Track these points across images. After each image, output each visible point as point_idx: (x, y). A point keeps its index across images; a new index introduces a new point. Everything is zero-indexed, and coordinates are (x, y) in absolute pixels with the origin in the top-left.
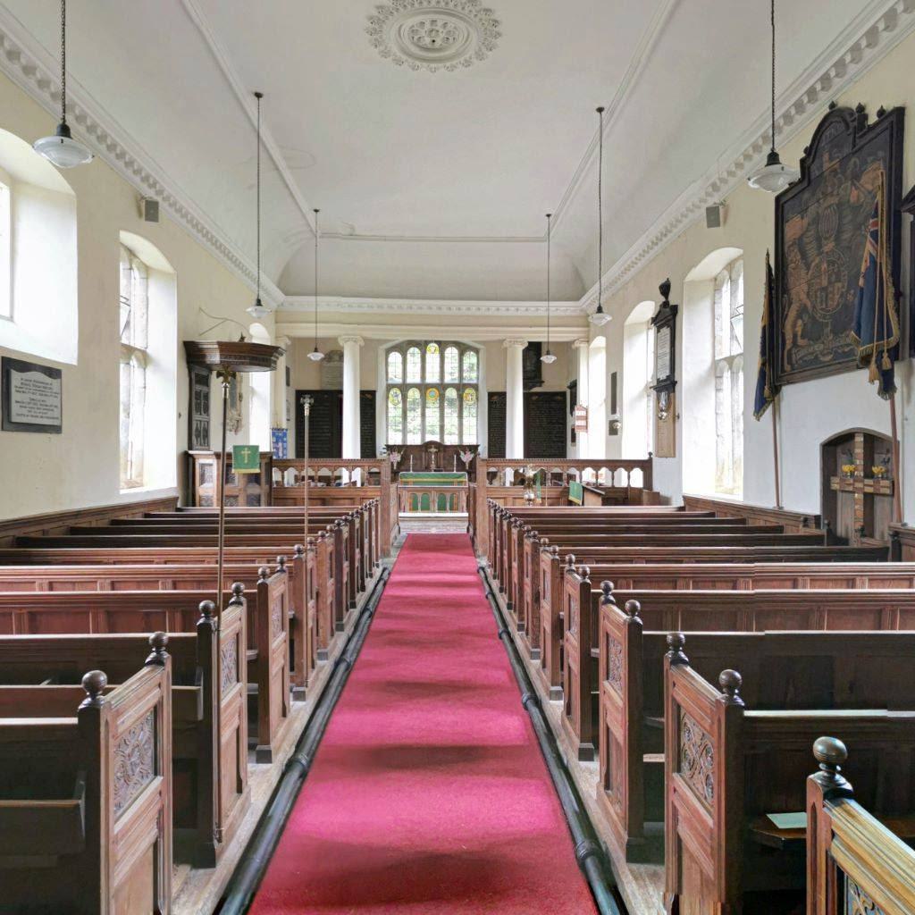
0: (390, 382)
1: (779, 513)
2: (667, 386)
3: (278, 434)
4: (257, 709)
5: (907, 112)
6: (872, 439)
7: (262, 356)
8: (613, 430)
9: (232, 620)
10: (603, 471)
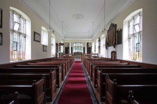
1: (108, 58)
2: (99, 47)
3: (64, 51)
4: (58, 83)
5: (117, 25)
6: (115, 51)
7: (63, 44)
8: (95, 51)
9: (60, 68)
10: (94, 55)
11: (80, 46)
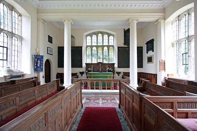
0: (87, 45)
11: (106, 43)
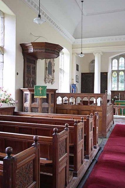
0: (113, 70)
3: (73, 86)
4: (73, 161)
